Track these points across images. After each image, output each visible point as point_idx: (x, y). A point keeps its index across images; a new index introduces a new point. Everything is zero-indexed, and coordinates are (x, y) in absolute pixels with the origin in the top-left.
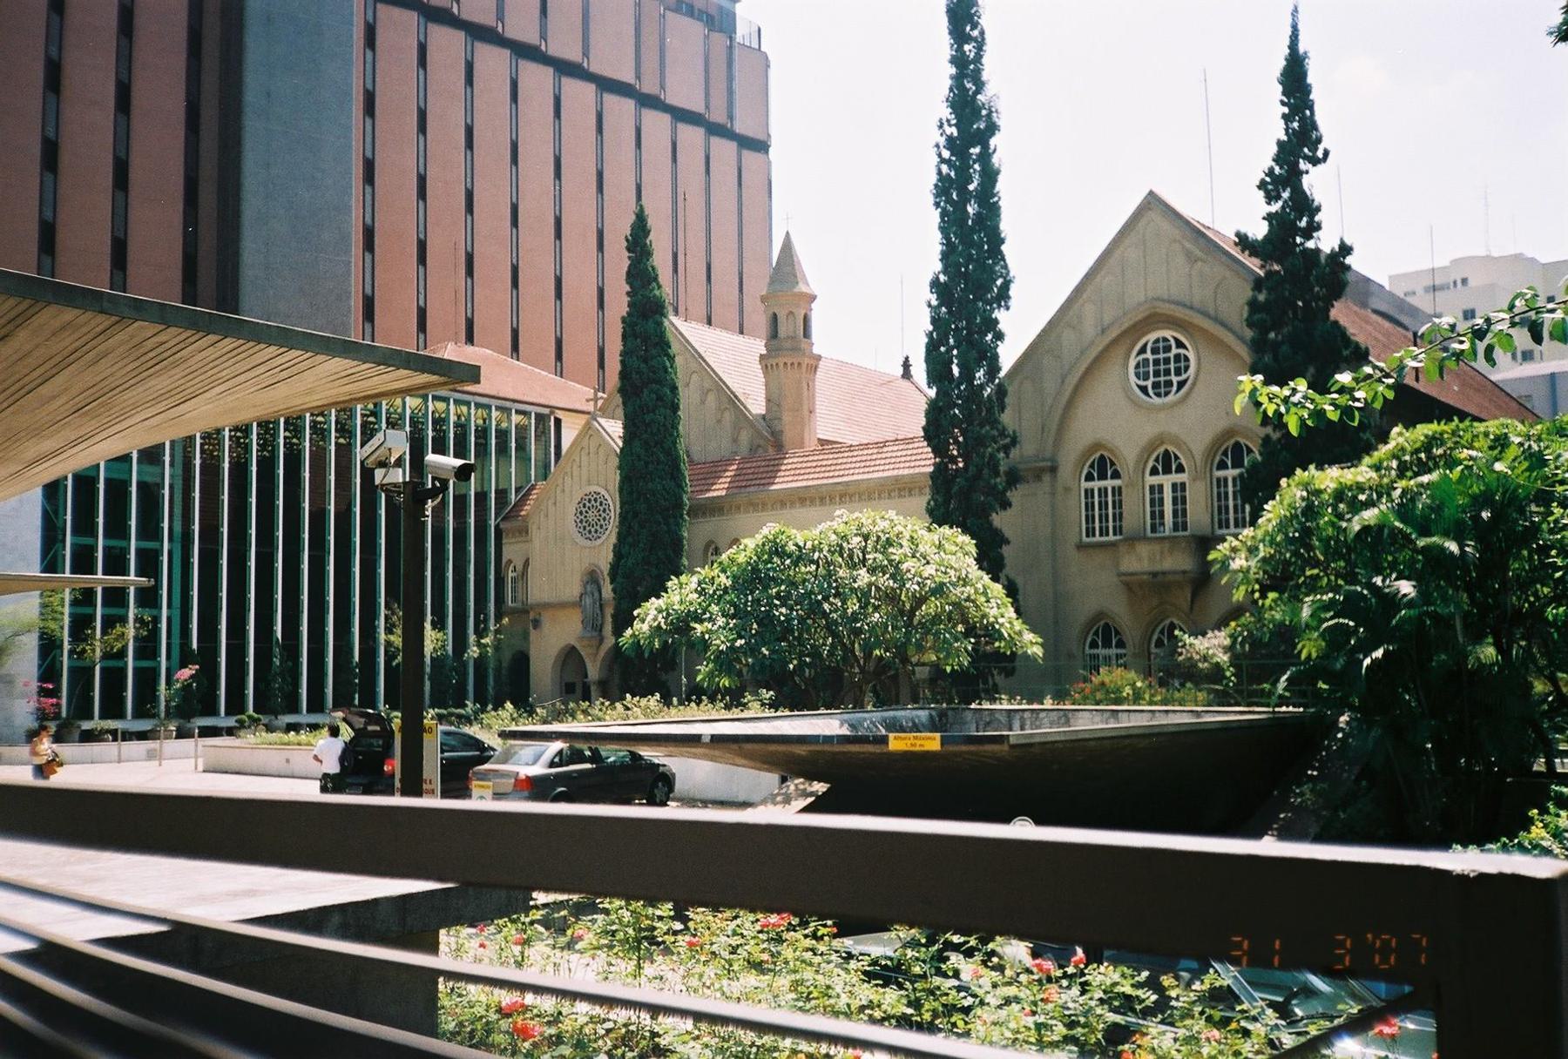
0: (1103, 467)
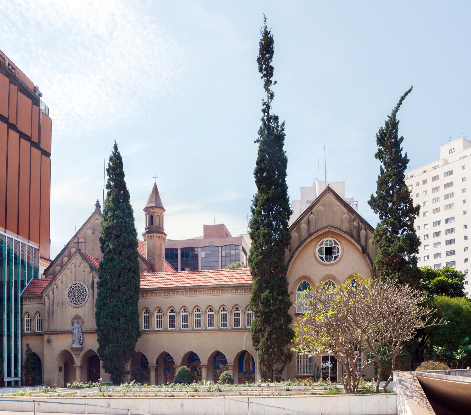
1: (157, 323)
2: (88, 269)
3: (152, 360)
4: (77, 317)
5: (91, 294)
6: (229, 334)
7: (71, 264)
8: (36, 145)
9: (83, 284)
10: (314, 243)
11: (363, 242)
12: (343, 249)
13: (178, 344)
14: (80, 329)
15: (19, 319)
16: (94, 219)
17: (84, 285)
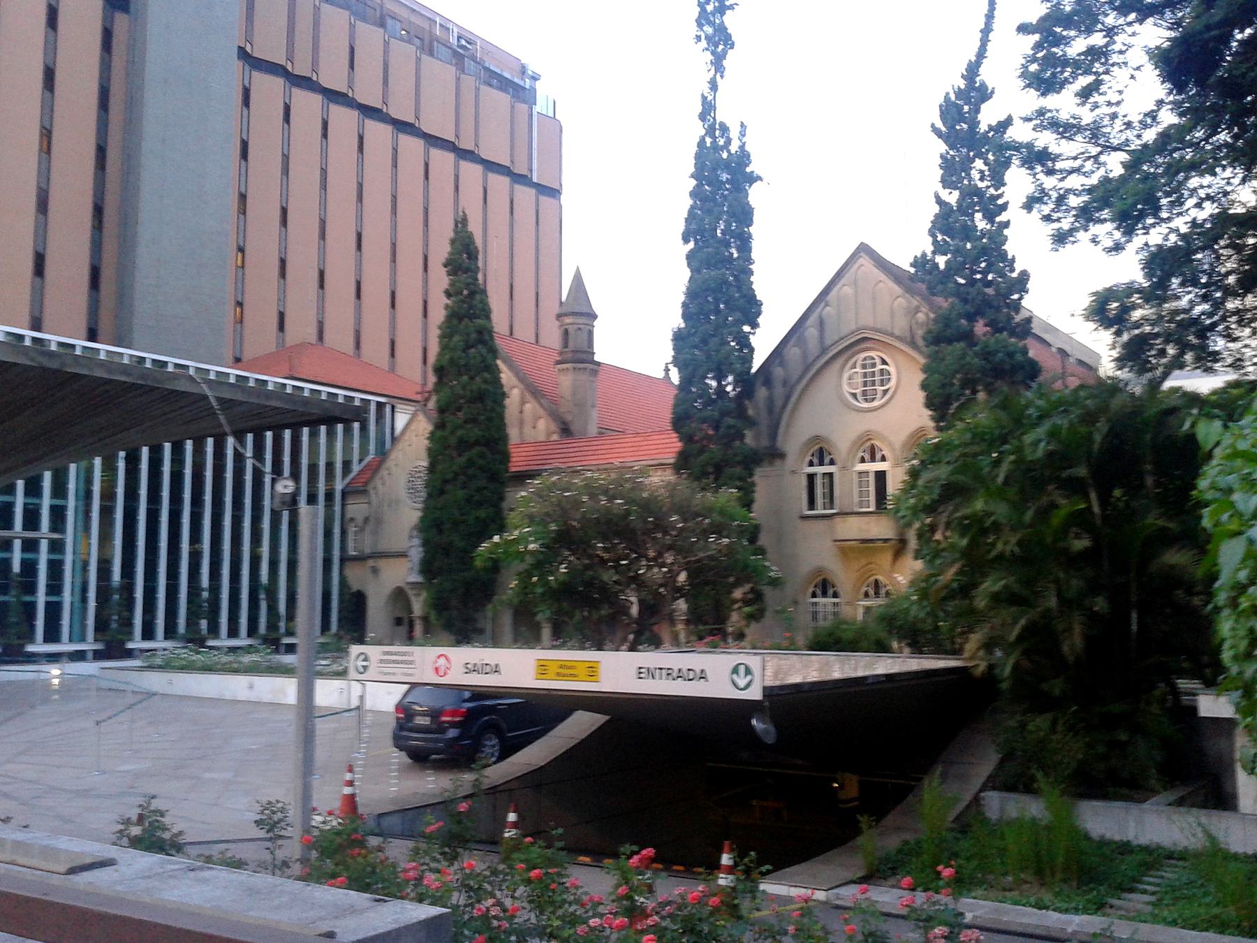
0: (822, 456)
8: (522, 179)
10: (840, 361)
12: (899, 373)
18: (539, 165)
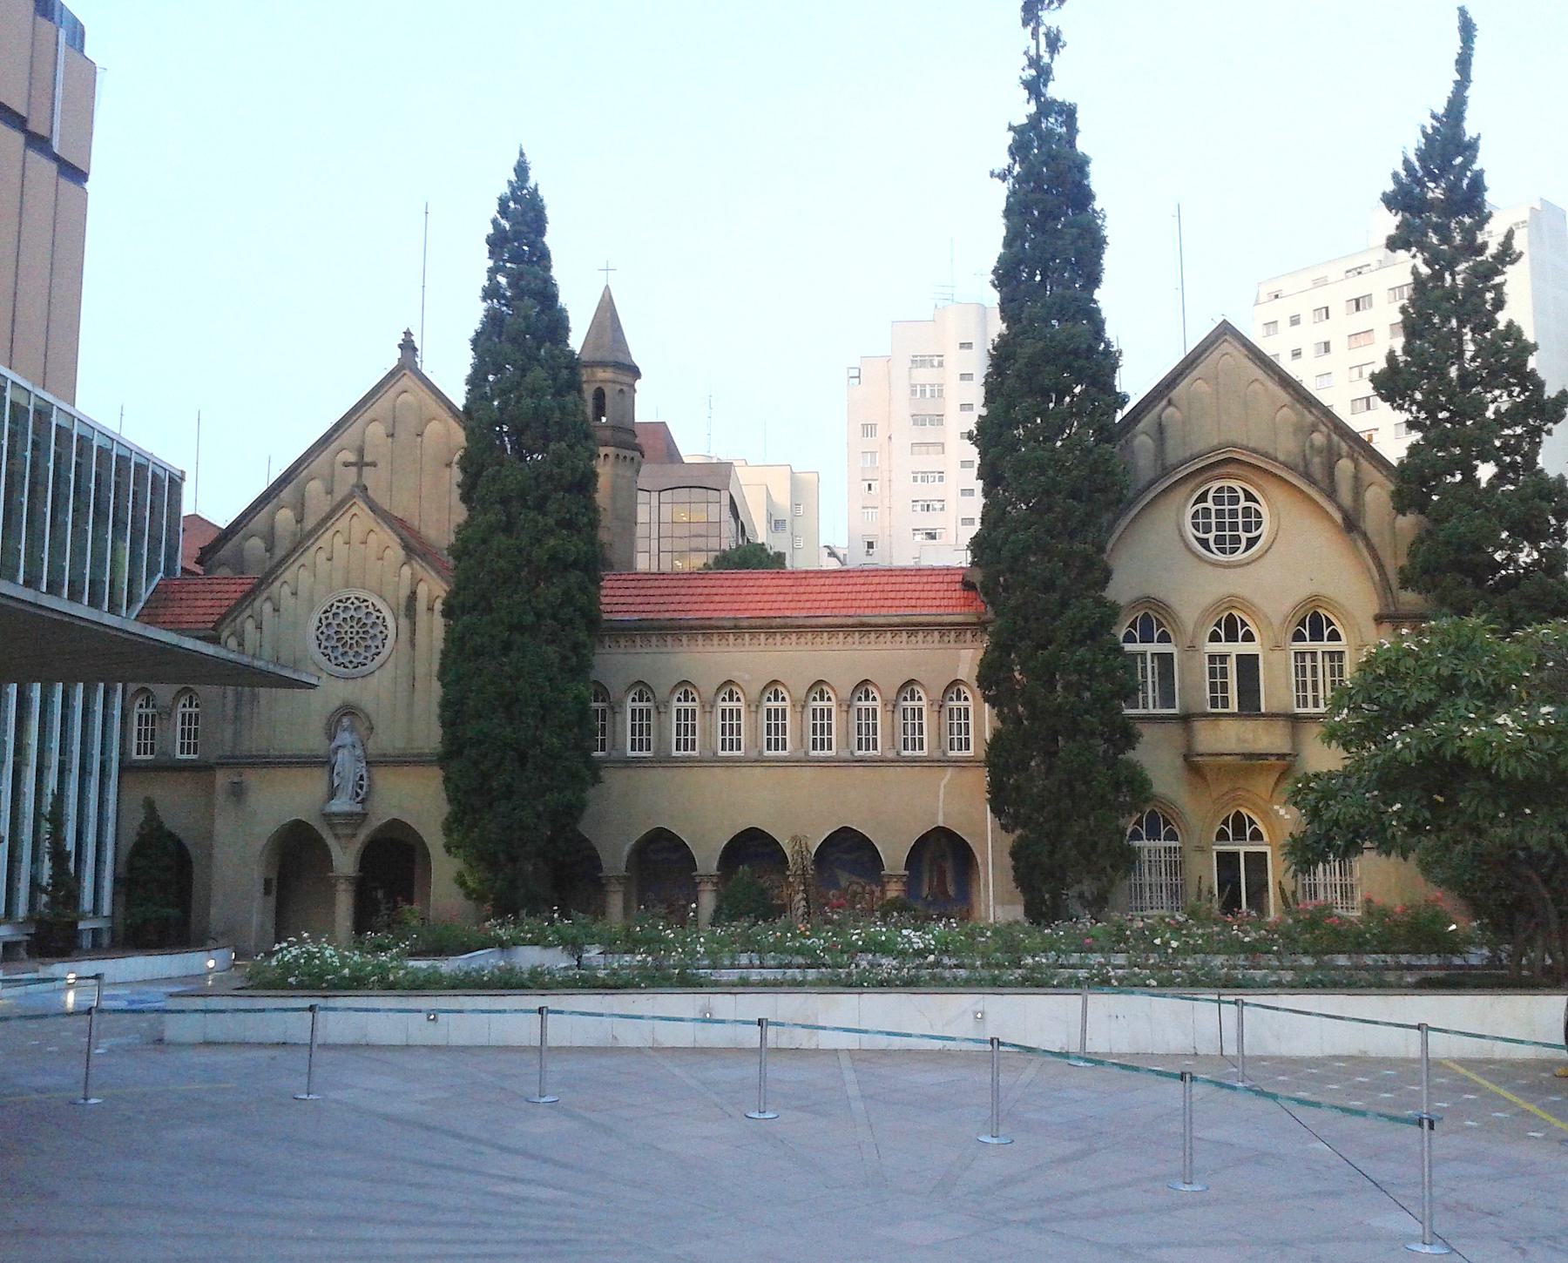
1: (633, 734)
2: (396, 552)
3: (615, 855)
4: (349, 710)
5: (404, 636)
6: (891, 773)
7: (330, 533)
8: (39, 142)
9: (373, 599)
11: (1345, 496)
13: (710, 807)
14: (359, 752)
15: (117, 712)
16: (392, 393)
17: (380, 605)
18: (63, 121)
